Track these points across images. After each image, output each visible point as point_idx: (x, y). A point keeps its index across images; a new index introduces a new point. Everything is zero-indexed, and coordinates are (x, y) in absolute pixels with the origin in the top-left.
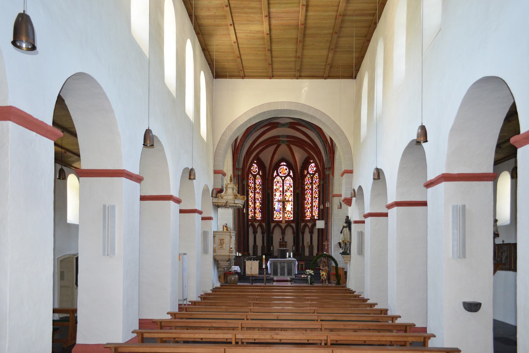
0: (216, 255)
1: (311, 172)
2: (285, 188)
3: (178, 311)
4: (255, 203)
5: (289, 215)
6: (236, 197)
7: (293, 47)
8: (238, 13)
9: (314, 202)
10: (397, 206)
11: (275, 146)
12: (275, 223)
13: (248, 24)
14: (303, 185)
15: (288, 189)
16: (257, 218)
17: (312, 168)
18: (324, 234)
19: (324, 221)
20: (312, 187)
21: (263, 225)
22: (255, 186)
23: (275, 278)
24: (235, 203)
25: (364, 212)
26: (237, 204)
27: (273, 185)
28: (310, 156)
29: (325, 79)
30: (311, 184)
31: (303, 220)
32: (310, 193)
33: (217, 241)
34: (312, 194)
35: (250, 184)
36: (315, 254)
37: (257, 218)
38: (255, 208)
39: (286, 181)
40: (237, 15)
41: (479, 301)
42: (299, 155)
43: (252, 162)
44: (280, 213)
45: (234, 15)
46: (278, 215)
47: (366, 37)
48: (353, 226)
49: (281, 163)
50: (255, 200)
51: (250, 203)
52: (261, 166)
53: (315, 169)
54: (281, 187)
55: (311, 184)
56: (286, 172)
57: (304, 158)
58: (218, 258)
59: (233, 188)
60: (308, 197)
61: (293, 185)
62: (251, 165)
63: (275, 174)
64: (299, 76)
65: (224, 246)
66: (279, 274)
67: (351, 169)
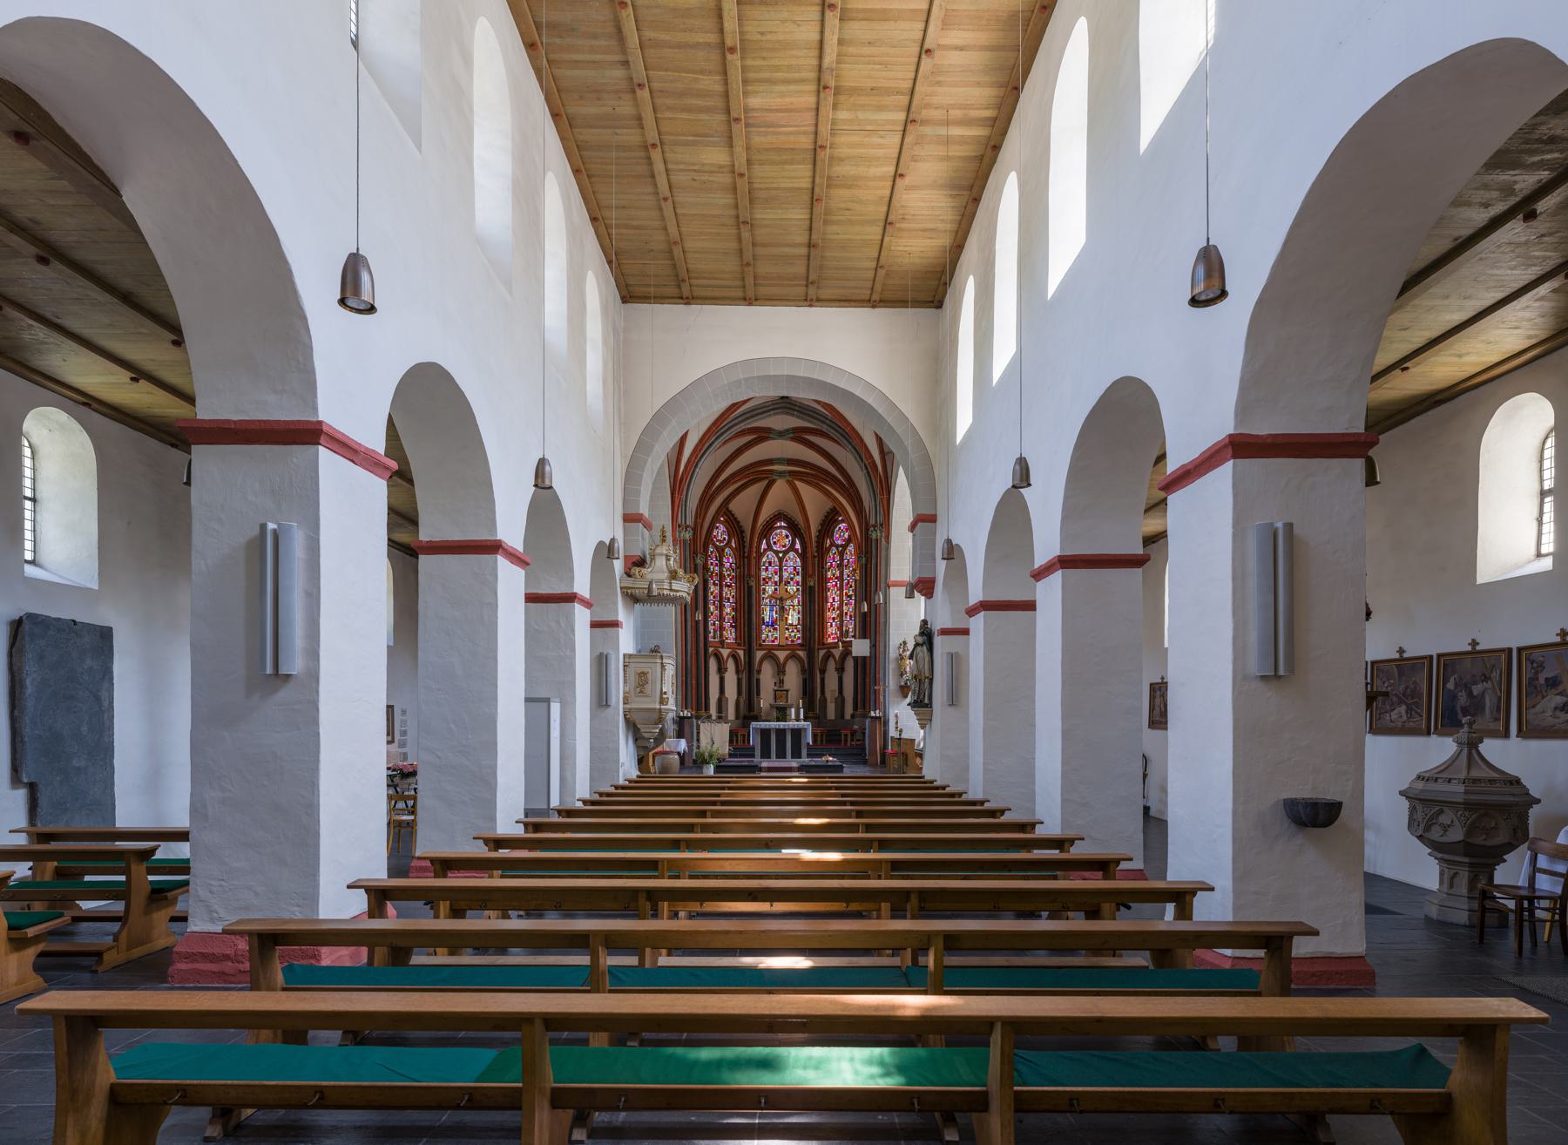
0: (630, 709)
1: (839, 542)
2: (785, 575)
3: (523, 832)
4: (721, 607)
5: (793, 634)
6: (673, 575)
7: (803, 217)
8: (670, 108)
9: (846, 604)
10: (1063, 568)
11: (766, 482)
12: (764, 650)
13: (694, 143)
14: (822, 568)
15: (792, 579)
16: (727, 639)
17: (841, 533)
18: (867, 671)
19: (868, 641)
20: (842, 573)
21: (738, 654)
22: (721, 572)
23: (765, 764)
24: (671, 590)
25: (968, 603)
26: (677, 591)
27: (760, 569)
28: (837, 507)
29: (874, 307)
30: (840, 566)
31: (824, 644)
32: (836, 585)
33: (632, 678)
34: (841, 589)
35: (712, 567)
36: (848, 716)
37: (727, 639)
38: (721, 619)
39: (787, 561)
40: (669, 115)
41: (1331, 796)
42: (814, 501)
43: (715, 520)
44: (775, 629)
45: (661, 116)
46: (770, 634)
47: (971, 190)
48: (938, 641)
49: (776, 523)
50: (721, 601)
51: (712, 608)
52: (734, 526)
53: (846, 535)
54: (776, 574)
55: (840, 566)
56: (787, 542)
57: (824, 513)
58: (635, 717)
59: (667, 556)
60: (833, 595)
61: (802, 569)
62: (712, 527)
63: (764, 546)
64: (815, 298)
65: (648, 688)
66: (773, 754)
67: (933, 513)
